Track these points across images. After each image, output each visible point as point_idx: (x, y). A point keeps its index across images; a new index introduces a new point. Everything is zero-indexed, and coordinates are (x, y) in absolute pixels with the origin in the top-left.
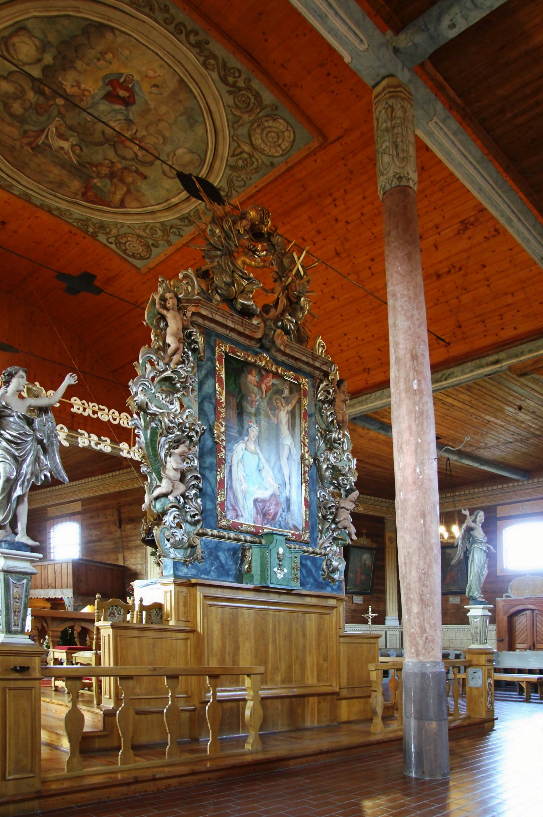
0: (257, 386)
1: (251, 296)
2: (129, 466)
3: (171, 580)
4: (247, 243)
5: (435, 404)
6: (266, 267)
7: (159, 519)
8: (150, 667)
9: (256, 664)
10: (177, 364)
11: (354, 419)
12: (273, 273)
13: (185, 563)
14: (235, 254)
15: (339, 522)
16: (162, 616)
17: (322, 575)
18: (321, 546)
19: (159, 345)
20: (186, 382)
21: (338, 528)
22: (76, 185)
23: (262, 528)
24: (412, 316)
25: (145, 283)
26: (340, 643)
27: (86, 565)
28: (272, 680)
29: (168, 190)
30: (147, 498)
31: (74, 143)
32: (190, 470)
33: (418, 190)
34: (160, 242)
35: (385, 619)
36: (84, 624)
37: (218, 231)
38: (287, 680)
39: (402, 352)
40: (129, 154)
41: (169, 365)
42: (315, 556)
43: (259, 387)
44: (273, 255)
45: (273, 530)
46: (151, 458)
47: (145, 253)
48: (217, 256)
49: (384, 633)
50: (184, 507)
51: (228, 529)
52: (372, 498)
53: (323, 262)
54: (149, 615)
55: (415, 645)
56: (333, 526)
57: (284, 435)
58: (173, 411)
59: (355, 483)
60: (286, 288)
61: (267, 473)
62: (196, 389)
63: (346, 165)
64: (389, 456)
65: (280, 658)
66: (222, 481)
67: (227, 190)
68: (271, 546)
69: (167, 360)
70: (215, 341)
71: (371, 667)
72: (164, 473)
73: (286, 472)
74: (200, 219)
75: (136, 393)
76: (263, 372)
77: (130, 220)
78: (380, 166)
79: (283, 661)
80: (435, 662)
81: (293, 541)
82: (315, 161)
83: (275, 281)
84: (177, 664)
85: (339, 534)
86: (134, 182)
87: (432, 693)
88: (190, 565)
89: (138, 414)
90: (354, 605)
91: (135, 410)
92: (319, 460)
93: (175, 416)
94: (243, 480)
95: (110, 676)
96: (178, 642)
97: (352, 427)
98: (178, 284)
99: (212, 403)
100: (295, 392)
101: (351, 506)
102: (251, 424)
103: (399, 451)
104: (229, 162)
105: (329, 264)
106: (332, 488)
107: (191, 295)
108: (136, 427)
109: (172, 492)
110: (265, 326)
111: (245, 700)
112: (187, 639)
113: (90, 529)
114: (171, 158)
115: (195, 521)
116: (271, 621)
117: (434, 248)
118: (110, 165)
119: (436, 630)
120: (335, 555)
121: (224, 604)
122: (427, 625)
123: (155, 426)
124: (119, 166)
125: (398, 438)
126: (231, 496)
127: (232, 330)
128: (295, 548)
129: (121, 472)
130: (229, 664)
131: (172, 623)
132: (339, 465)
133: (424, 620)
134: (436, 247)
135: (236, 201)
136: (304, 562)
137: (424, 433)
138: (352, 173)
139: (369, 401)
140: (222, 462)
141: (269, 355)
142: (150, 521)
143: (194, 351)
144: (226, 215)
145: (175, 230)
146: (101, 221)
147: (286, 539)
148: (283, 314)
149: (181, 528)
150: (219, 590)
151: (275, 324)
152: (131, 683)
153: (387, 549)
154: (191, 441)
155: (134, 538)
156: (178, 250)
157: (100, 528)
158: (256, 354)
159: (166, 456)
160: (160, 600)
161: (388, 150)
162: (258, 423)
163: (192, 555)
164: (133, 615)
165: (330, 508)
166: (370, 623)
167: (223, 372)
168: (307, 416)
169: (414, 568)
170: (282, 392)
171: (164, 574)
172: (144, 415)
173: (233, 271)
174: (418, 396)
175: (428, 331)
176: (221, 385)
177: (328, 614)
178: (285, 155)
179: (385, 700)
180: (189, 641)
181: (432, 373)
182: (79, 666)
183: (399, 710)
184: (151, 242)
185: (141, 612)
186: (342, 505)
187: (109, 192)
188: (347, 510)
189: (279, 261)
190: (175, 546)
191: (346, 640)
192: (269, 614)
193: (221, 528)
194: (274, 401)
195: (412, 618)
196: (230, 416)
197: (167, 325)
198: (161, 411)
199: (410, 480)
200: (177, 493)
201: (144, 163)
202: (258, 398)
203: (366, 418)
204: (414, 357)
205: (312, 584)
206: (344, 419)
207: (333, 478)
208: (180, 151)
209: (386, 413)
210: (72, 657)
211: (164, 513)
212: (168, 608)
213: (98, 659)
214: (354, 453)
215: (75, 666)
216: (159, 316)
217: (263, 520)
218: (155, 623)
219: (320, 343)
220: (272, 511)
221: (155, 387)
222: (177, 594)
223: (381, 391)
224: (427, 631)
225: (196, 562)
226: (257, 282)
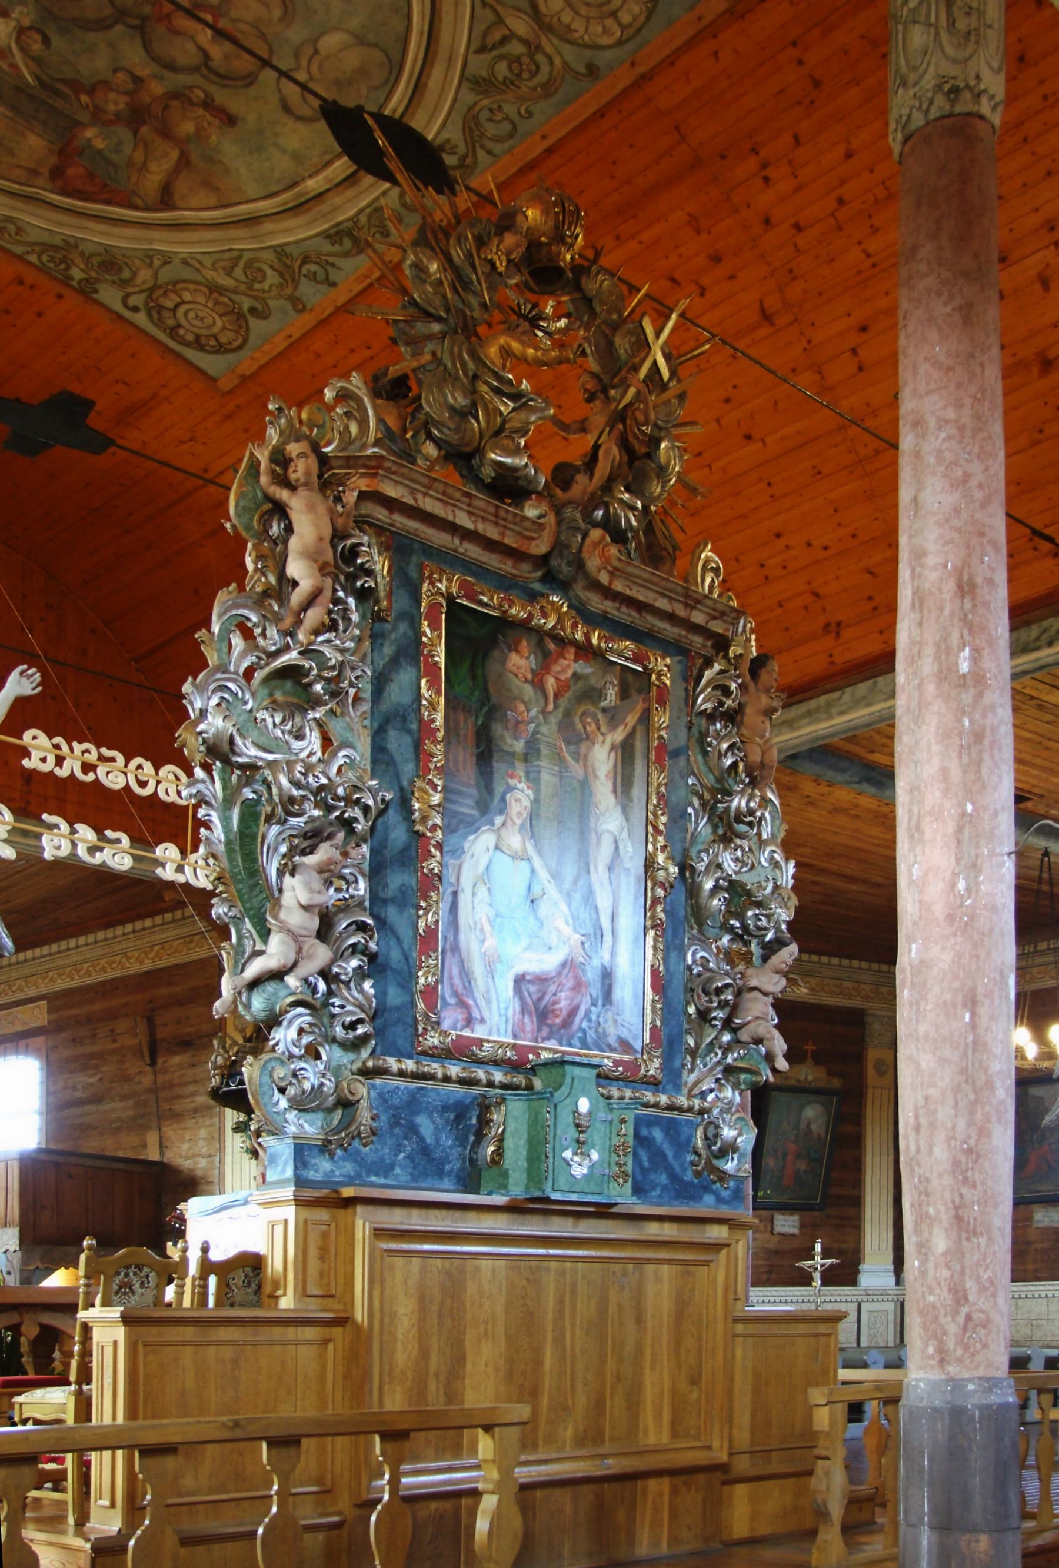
0: (532, 682)
1: (522, 442)
2: (181, 905)
3: (289, 1192)
4: (514, 297)
5: (1016, 710)
6: (568, 361)
7: (258, 1037)
8: (224, 1419)
9: (509, 1400)
10: (317, 632)
11: (792, 759)
12: (585, 378)
13: (325, 1148)
14: (482, 330)
15: (742, 1026)
16: (259, 1287)
17: (692, 1163)
18: (691, 1090)
19: (268, 582)
20: (338, 678)
21: (738, 1041)
22: (34, 145)
23: (535, 1050)
24: (967, 477)
25: (229, 417)
26: (735, 1336)
27: (57, 1165)
28: (551, 1439)
29: (297, 157)
30: (227, 985)
31: (26, 22)
32: (345, 907)
33: (1004, 123)
34: (271, 303)
35: (857, 1272)
36: (47, 1319)
37: (434, 267)
38: (591, 1436)
39: (931, 577)
40: (184, 53)
41: (292, 634)
42: (675, 1115)
43: (538, 684)
44: (587, 329)
45: (564, 1053)
46: (241, 881)
47: (230, 335)
48: (430, 337)
49: (855, 1305)
50: (326, 1004)
51: (445, 1054)
52: (835, 961)
53: (724, 342)
54: (224, 1286)
55: (938, 1336)
56: (726, 1038)
57: (602, 808)
58: (303, 755)
59: (789, 924)
60: (621, 416)
61: (551, 909)
62: (367, 695)
63: (800, 62)
64: (884, 851)
65: (573, 1379)
66: (431, 933)
67: (462, 149)
68: (558, 1096)
69: (288, 622)
70: (421, 567)
71: (817, 1396)
72: (275, 917)
73: (604, 902)
74: (386, 234)
75: (203, 713)
76: (549, 645)
77: (188, 244)
78: (899, 61)
79: (579, 1390)
80: (988, 1379)
81: (617, 1079)
82: (716, 54)
83: (591, 398)
84: (297, 1409)
85: (741, 1058)
86: (200, 133)
87: (979, 1461)
88: (339, 1152)
89: (207, 768)
90: (776, 1239)
91: (198, 757)
92: (693, 870)
93: (309, 769)
94: (487, 927)
95: (113, 1448)
96: (303, 1352)
97: (786, 779)
98: (321, 417)
99: (409, 732)
100: (633, 692)
101: (776, 984)
102: (512, 782)
103: (912, 837)
104: (470, 70)
105: (740, 345)
106: (726, 939)
107: (358, 444)
108: (202, 801)
109: (294, 965)
110: (559, 523)
111: (475, 1494)
112: (325, 1342)
113: (71, 1072)
114: (304, 63)
115: (357, 1038)
116: (552, 1287)
117: (1038, 286)
118: (131, 86)
119: (994, 1295)
120: (728, 1111)
121: (426, 1247)
122: (970, 1284)
123: (251, 796)
124: (157, 89)
125: (911, 803)
126: (455, 971)
127: (468, 535)
128: (622, 1098)
129: (158, 919)
130: (435, 1398)
131: (287, 1302)
132: (748, 879)
133: (962, 1272)
134: (1045, 283)
135: (486, 180)
136: (644, 1132)
137: (984, 787)
138: (817, 84)
139: (834, 710)
140: (431, 882)
141: (568, 599)
142: (235, 1043)
143: (364, 595)
144: (458, 222)
145: (313, 267)
146: (107, 249)
147: (599, 1076)
148: (607, 487)
149: (318, 1057)
150: (415, 1212)
151: (587, 515)
152: (170, 1462)
153: (870, 1093)
154: (351, 831)
155: (191, 1088)
156: (322, 323)
157: (97, 1066)
158: (532, 597)
159: (280, 874)
160: (257, 1245)
161: (923, 11)
162: (533, 780)
163: (345, 1125)
164: (181, 1286)
165: (719, 991)
166: (817, 1282)
167: (441, 649)
168: (665, 754)
169: (941, 1137)
170: (601, 694)
171: (268, 1179)
172: (223, 771)
173: (475, 377)
174: (972, 691)
175: (1008, 515)
176: (433, 683)
177: (706, 1263)
178: (627, 41)
179: (851, 1482)
180: (331, 1346)
181: (1013, 629)
182: (30, 1426)
183: (889, 1505)
184: (246, 303)
185: (204, 1277)
186: (753, 983)
187: (130, 164)
188: (766, 994)
189: (602, 342)
190: (300, 1105)
191: (751, 1328)
192: (548, 1269)
193: (424, 1053)
194: (577, 720)
195: (931, 1265)
196: (456, 761)
197: (289, 530)
198: (270, 757)
199: (939, 910)
200: (309, 967)
201: (225, 79)
202: (534, 712)
203: (825, 754)
204: (966, 588)
205: (664, 1188)
206: (767, 760)
207: (730, 913)
208: (330, 42)
209: (880, 740)
210: (12, 1406)
211: (273, 1021)
212: (278, 1265)
213: (84, 1406)
214: (789, 847)
215: (20, 1428)
216: (268, 506)
217: (539, 1030)
218: (241, 1305)
219: (708, 561)
220: (563, 1005)
221: (253, 695)
222: (303, 1229)
223: (870, 682)
224: (971, 1299)
225: (356, 1143)
226: (540, 403)
